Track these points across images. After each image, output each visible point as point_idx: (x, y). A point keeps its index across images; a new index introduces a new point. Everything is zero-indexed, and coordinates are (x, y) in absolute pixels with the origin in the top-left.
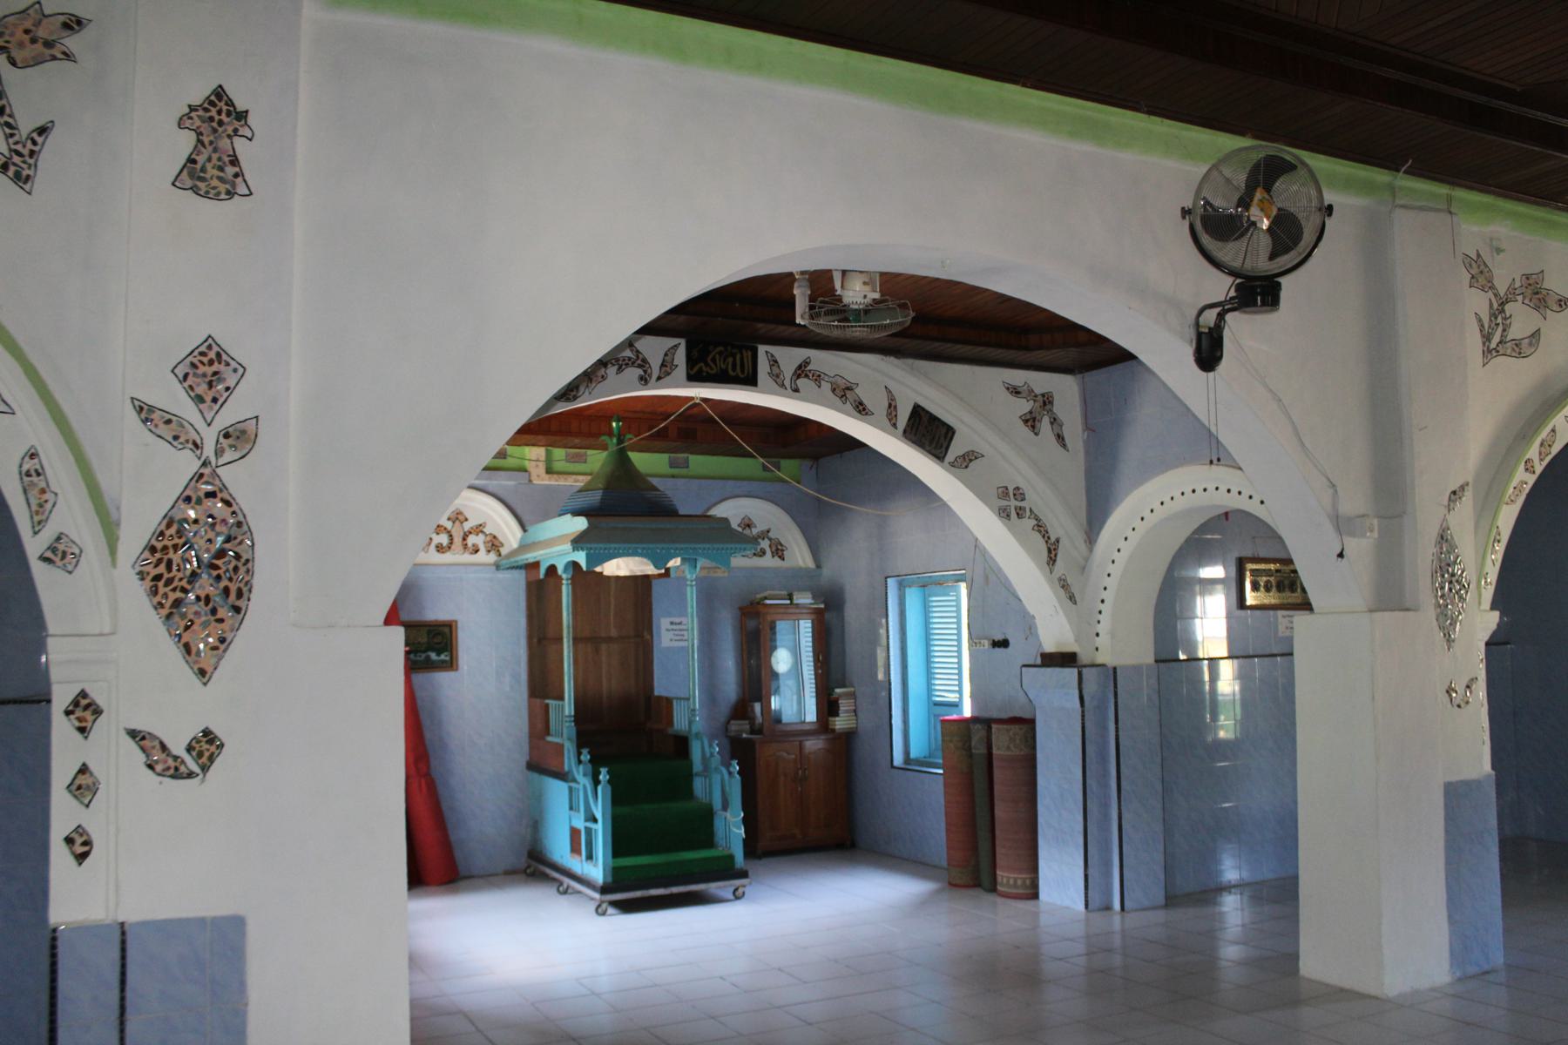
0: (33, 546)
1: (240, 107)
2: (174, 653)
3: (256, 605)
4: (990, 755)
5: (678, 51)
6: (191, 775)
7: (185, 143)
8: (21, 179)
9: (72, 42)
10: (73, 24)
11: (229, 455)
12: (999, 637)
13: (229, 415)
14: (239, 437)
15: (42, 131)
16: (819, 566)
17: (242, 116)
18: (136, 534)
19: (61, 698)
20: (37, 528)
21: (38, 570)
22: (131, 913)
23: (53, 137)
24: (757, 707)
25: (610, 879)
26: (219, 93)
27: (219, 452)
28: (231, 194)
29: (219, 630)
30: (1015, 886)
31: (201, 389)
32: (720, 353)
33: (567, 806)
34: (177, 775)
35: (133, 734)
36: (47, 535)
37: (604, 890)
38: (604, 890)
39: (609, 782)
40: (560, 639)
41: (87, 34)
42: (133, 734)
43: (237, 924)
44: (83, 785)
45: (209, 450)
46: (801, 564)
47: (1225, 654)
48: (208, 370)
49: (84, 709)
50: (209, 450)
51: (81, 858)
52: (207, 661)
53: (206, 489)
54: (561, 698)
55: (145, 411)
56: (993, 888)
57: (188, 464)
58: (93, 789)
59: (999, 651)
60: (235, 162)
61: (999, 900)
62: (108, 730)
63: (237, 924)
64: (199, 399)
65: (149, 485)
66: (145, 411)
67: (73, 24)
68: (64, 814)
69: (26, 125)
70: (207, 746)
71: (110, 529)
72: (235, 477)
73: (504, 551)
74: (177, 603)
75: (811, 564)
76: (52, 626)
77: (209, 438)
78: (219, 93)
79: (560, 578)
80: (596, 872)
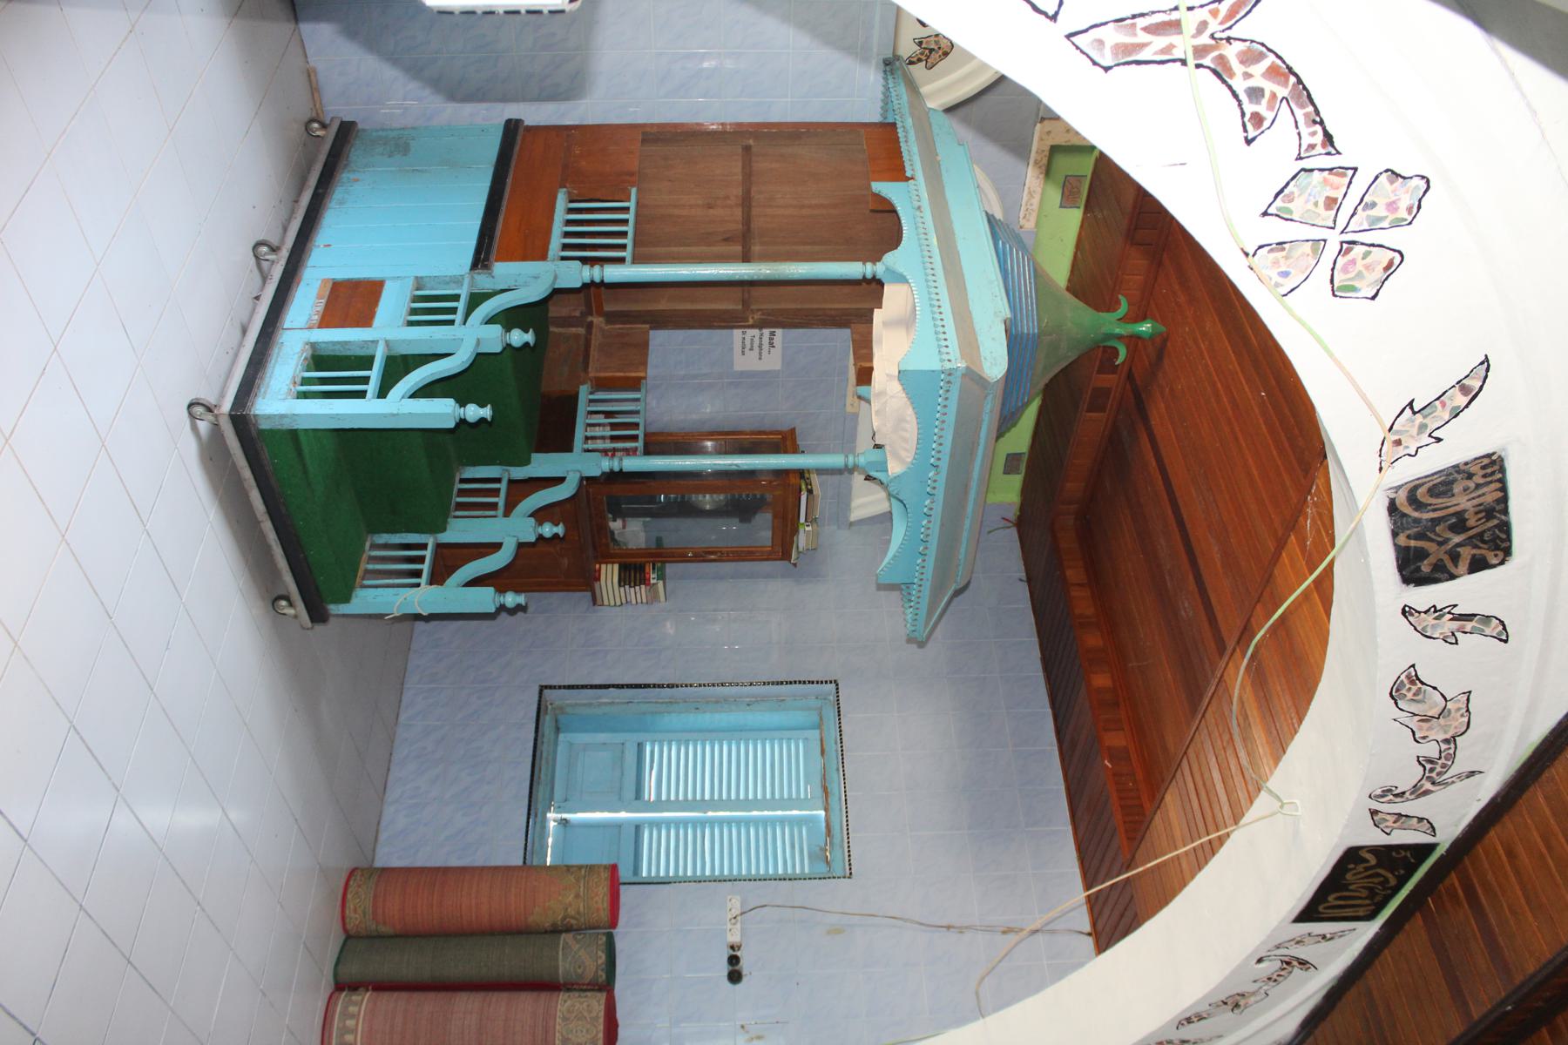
4: (550, 986)
12: (745, 965)
16: (851, 524)
19: (1364, 482)
25: (264, 425)
30: (344, 1030)
32: (1387, 880)
37: (241, 421)
38: (241, 421)
39: (462, 422)
40: (746, 258)
46: (854, 504)
54: (637, 260)
56: (343, 986)
59: (724, 969)
61: (321, 1005)
73: (918, 71)
75: (855, 515)
79: (876, 258)
80: (279, 402)
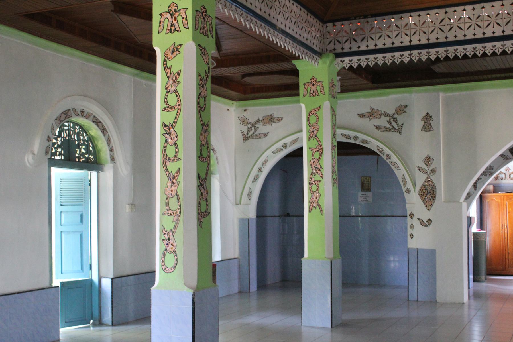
0: (404, 190)
1: (431, 115)
2: (424, 206)
3: (437, 198)
5: (477, 209)
6: (427, 226)
7: (422, 123)
8: (400, 133)
9: (406, 110)
10: (406, 106)
11: (432, 174)
13: (431, 168)
14: (433, 171)
15: (402, 124)
17: (431, 117)
18: (418, 187)
20: (405, 186)
21: (405, 193)
22: (419, 247)
23: (404, 125)
24: (370, 200)
26: (427, 114)
27: (430, 174)
28: (430, 130)
29: (430, 203)
31: (427, 163)
33: (347, 31)
34: (425, 226)
35: (418, 219)
36: (406, 188)
41: (408, 107)
42: (418, 219)
43: (435, 250)
44: (412, 227)
45: (429, 174)
47: (277, 214)
48: (428, 160)
49: (412, 215)
50: (429, 174)
51: (412, 238)
52: (430, 208)
53: (429, 180)
55: (419, 168)
57: (425, 176)
58: (413, 227)
60: (430, 125)
62: (415, 218)
63: (435, 250)
64: (427, 165)
65: (421, 179)
66: (419, 168)
67: (406, 106)
68: (410, 231)
69: (400, 124)
70: (430, 221)
71: (414, 185)
72: (433, 178)
74: (425, 198)
76: (407, 202)
77: (429, 172)
78: (427, 114)
